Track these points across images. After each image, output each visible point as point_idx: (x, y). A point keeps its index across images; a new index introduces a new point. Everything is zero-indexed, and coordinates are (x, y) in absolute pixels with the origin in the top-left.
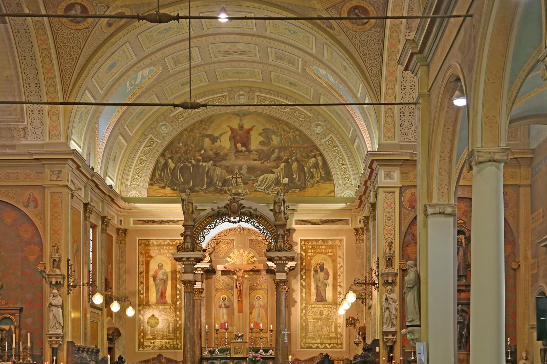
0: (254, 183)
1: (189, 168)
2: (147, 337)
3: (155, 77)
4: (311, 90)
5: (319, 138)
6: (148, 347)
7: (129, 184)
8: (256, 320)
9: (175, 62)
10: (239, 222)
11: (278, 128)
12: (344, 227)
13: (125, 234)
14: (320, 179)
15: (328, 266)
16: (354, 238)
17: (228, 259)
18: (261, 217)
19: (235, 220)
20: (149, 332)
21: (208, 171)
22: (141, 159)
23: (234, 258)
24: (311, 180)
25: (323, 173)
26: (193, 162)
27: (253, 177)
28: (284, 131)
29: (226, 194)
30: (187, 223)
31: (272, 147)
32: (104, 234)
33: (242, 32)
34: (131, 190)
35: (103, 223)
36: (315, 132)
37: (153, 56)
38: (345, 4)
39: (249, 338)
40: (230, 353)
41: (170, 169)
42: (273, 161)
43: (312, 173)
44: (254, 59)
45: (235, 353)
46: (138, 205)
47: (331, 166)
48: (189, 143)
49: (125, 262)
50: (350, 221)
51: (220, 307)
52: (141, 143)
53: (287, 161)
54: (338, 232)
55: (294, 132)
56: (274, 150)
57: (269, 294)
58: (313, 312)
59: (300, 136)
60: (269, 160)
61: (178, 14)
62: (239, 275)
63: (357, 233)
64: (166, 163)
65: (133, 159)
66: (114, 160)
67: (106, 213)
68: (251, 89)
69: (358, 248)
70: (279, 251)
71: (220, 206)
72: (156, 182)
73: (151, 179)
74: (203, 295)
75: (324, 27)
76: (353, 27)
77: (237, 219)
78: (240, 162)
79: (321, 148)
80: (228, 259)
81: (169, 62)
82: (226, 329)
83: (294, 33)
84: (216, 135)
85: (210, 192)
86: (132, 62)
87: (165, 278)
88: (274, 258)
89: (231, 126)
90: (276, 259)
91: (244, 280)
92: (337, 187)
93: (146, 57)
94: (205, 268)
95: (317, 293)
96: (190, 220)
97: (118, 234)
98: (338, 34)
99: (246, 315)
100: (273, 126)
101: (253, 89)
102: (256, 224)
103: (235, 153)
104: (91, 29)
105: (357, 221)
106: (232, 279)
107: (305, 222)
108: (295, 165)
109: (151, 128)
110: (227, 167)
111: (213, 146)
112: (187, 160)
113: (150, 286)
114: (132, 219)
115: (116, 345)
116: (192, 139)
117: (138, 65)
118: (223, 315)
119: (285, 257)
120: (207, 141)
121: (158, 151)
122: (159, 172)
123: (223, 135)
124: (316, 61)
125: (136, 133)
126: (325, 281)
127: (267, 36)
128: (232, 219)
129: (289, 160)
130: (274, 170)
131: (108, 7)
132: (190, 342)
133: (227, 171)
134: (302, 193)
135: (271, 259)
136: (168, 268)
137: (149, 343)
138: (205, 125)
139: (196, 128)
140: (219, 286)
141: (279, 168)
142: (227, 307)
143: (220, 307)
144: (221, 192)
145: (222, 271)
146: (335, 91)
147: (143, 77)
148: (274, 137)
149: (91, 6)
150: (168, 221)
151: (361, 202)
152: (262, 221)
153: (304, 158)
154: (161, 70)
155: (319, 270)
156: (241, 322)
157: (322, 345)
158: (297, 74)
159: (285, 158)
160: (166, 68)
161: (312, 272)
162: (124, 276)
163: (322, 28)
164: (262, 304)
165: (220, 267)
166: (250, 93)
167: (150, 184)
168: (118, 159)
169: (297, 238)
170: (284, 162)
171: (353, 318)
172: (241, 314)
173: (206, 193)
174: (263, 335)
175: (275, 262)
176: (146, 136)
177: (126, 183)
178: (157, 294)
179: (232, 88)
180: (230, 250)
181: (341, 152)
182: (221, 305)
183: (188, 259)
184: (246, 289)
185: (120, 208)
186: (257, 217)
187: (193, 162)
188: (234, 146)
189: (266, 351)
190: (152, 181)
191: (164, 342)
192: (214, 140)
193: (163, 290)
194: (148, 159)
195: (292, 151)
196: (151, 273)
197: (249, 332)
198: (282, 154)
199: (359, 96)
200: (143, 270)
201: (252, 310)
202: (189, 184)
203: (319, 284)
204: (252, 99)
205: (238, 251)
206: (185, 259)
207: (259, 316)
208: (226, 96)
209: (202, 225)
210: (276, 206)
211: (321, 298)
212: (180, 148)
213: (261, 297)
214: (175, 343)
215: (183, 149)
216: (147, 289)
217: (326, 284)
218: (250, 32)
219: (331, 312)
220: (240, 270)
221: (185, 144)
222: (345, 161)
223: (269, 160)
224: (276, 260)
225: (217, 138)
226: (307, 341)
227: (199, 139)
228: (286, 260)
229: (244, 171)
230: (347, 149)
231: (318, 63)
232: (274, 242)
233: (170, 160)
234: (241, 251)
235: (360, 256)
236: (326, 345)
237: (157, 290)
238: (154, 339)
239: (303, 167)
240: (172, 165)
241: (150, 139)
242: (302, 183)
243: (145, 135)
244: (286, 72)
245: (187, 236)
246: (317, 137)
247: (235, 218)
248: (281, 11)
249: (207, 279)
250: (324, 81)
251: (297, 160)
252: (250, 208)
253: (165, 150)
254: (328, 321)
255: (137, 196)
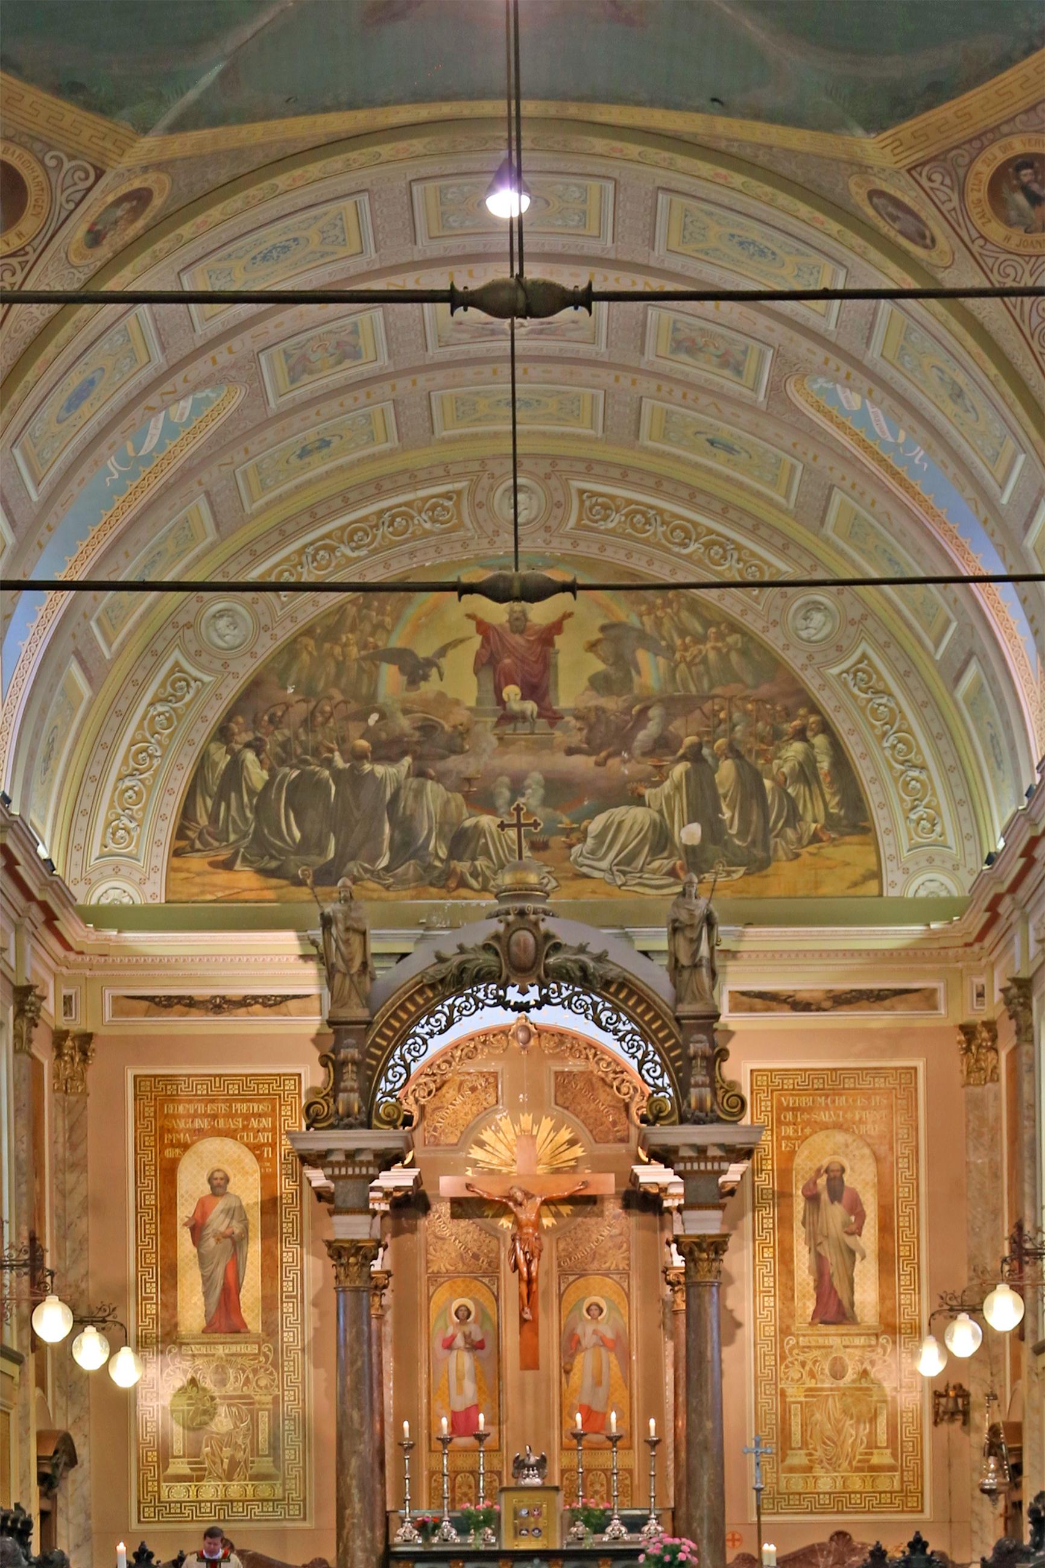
0: (571, 846)
1: (321, 786)
2: (171, 1471)
3: (213, 426)
4: (793, 468)
5: (819, 658)
6: (176, 1508)
7: (96, 851)
8: (585, 1401)
9: (291, 369)
10: (539, 1006)
11: (658, 623)
12: (922, 1020)
13: (84, 1053)
14: (824, 827)
15: (861, 1178)
16: (955, 1062)
17: (476, 1153)
18: (622, 986)
19: (524, 999)
20: (178, 1447)
21: (395, 796)
22: (140, 752)
23: (501, 1147)
24: (790, 833)
25: (833, 801)
26: (339, 762)
27: (565, 821)
28: (683, 632)
29: (463, 892)
30: (344, 1014)
31: (637, 700)
32: (25, 1058)
33: (559, 249)
34: (104, 877)
35: (20, 1013)
36: (804, 634)
37: (223, 347)
38: (982, 149)
39: (563, 1472)
40: (497, 1533)
41: (251, 792)
42: (644, 754)
43: (792, 802)
44: (585, 350)
45: (517, 1533)
46: (140, 940)
47: (864, 770)
48: (321, 685)
49: (85, 1169)
50: (941, 996)
51: (449, 1345)
52: (141, 687)
53: (695, 755)
54: (895, 1040)
55: (720, 637)
56: (644, 711)
57: (635, 1294)
58: (803, 1364)
59: (744, 653)
60: (629, 750)
61: (590, 285)
62: (523, 1217)
63: (969, 1042)
64: (236, 766)
65: (110, 749)
66: (48, 758)
67: (28, 974)
68: (553, 464)
69: (976, 1104)
70: (698, 1122)
71: (469, 945)
72: (198, 845)
73: (180, 833)
74: (388, 1297)
75: (892, 233)
76: (1007, 239)
77: (533, 995)
78: (517, 760)
79: (826, 701)
80: (476, 1153)
81: (272, 370)
82: (480, 1438)
83: (762, 253)
84: (424, 651)
85: (402, 882)
86: (145, 376)
87: (237, 1228)
88: (674, 1150)
89: (480, 615)
90: (684, 1153)
91: (545, 1240)
92: (891, 858)
93: (198, 353)
94: (397, 1189)
95: (819, 1287)
96: (355, 1000)
97: (60, 1056)
98: (947, 261)
99: (549, 1379)
100: (640, 615)
101: (563, 465)
102: (603, 1017)
103: (498, 724)
104: (32, 257)
105: (970, 994)
106: (495, 1234)
107: (770, 1000)
108: (726, 771)
109: (175, 625)
110: (469, 780)
111: (413, 695)
112: (316, 752)
113: (180, 1264)
114: (108, 993)
115: (61, 1502)
116: (332, 669)
117: (167, 387)
118: (460, 1379)
119: (721, 1146)
120: (389, 676)
121: (204, 719)
122: (209, 802)
123: (451, 653)
124: (835, 361)
125: (123, 645)
126: (850, 1240)
127: (653, 263)
128: (513, 995)
129: (705, 751)
130: (648, 793)
131: (100, 174)
132: (362, 1489)
133: (467, 796)
134: (755, 883)
135: (664, 1156)
136: (247, 1190)
137: (179, 1492)
138: (381, 611)
139: (349, 622)
140: (442, 1261)
141: (668, 783)
142: (475, 1346)
143: (449, 1345)
144: (447, 881)
145: (456, 1202)
146: (895, 474)
147: (170, 429)
148: (643, 657)
149: (39, 171)
150: (245, 1002)
151: (994, 917)
152: (625, 1000)
153: (762, 741)
154: (239, 396)
155: (825, 1196)
156: (530, 1407)
157: (840, 1501)
158: (752, 408)
159: (689, 740)
160: (258, 394)
161: (799, 1204)
162: (83, 1225)
163: (886, 238)
164: (610, 1335)
165: (448, 1185)
166: (553, 482)
167: (177, 853)
168: (59, 753)
169: (738, 1069)
170: (684, 758)
171: (959, 1388)
172: (529, 1374)
173: (387, 888)
174: (614, 1459)
175: (681, 1167)
176: (158, 657)
177: (84, 848)
178: (206, 1294)
179: (483, 461)
180: (484, 1117)
181: (904, 717)
182: (453, 1338)
183: (351, 1156)
184: (547, 1273)
185: (67, 947)
186: (607, 984)
187: (339, 762)
188: (491, 696)
189: (635, 1525)
190: (184, 840)
191: (235, 1489)
192: (416, 670)
193: (231, 1276)
194: (165, 749)
195: (715, 714)
196: (185, 1211)
197: (563, 1448)
198: (677, 726)
199: (1004, 500)
200: (151, 1200)
201: (573, 1356)
202: (322, 850)
203: (827, 1250)
204: (558, 505)
205: (515, 1121)
206: (341, 1158)
207: (598, 1383)
208: (459, 493)
209: (399, 1019)
210: (681, 941)
211: (834, 1310)
212: (288, 706)
213: (603, 1304)
214: (279, 1493)
215: (301, 710)
216: (169, 1275)
217: (852, 1253)
218: (592, 248)
219: (873, 1363)
220: (528, 1196)
221: (308, 692)
222: (919, 752)
223: (629, 750)
224: (684, 1160)
225: (429, 663)
226: (783, 1483)
227: (360, 668)
228: (721, 1159)
229: (532, 798)
230: (925, 704)
231: (845, 368)
232: (672, 1084)
233: (250, 756)
234: (526, 1120)
235: (980, 1135)
236: (856, 1498)
237: (207, 1281)
238: (200, 1479)
239: (758, 777)
240: (256, 774)
241: (172, 672)
242: (754, 843)
243: (154, 653)
244: (704, 400)
245: (344, 1063)
246: (810, 657)
247: (523, 992)
248: (723, 171)
249: (397, 1232)
250: (853, 435)
251: (734, 752)
252: (582, 949)
253: (230, 715)
254: (864, 1397)
255: (126, 900)
